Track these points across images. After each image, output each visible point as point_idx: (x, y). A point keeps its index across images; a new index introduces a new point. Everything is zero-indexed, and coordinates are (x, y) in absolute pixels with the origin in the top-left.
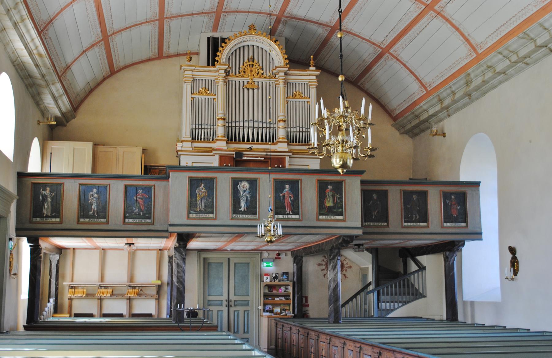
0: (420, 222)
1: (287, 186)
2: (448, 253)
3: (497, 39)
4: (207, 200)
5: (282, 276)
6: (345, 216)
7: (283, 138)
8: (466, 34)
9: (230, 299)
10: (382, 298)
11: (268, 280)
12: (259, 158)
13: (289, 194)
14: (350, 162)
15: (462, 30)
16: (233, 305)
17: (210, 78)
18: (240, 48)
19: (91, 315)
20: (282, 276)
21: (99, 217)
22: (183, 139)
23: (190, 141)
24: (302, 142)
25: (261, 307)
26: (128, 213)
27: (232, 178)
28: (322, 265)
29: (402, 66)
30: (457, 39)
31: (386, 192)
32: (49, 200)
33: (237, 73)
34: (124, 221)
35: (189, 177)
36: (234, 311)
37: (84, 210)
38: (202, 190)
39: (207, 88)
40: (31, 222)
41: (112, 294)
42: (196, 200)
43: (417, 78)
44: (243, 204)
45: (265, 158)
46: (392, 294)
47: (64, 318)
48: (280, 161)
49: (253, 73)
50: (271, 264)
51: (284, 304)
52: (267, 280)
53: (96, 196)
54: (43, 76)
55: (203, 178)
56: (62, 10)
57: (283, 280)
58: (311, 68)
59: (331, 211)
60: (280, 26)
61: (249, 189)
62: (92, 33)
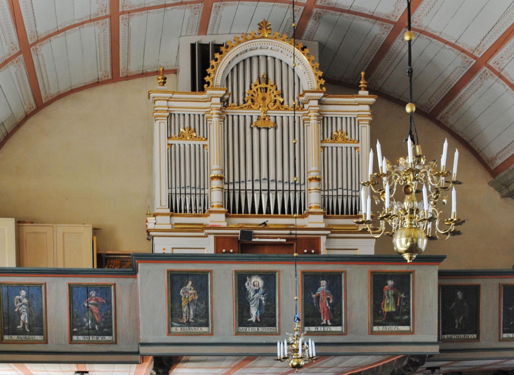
1: (323, 283)
4: (197, 305)
7: (316, 207)
12: (278, 240)
13: (327, 294)
14: (423, 242)
18: (244, 61)
21: (32, 333)
23: (167, 214)
31: (477, 288)
33: (241, 102)
34: (71, 339)
35: (169, 272)
38: (189, 291)
42: (181, 307)
44: (254, 311)
45: (288, 239)
48: (313, 243)
49: (267, 101)
53: (25, 301)
58: (361, 93)
59: (391, 319)
60: (311, 23)
61: (264, 288)
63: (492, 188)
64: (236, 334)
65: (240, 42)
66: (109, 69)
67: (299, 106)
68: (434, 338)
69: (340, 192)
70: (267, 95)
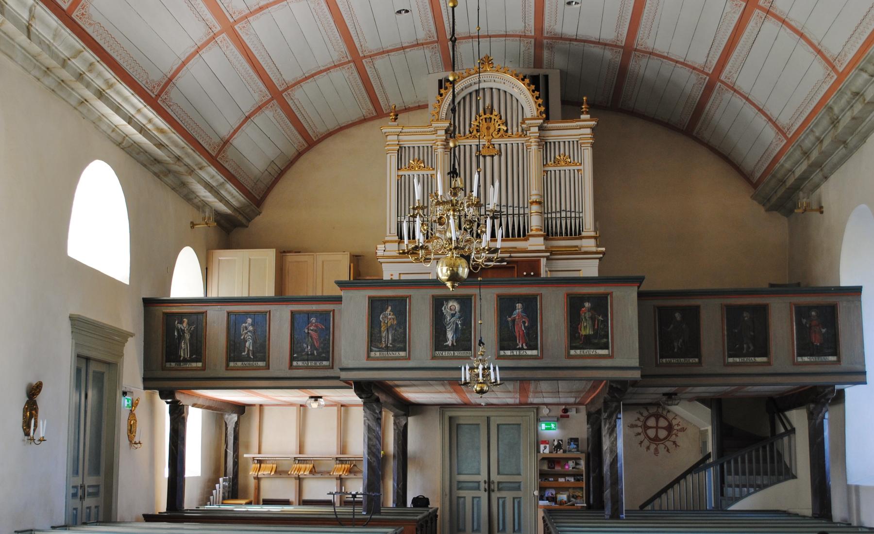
0: (755, 356)
2: (812, 406)
3: (858, 46)
4: (396, 330)
5: (569, 444)
6: (409, 352)
7: (537, 230)
8: (816, 43)
9: (492, 479)
10: (729, 479)
11: (547, 451)
14: (463, 271)
15: (808, 36)
16: (496, 489)
17: (425, 144)
18: (471, 94)
19: (286, 502)
20: (569, 444)
21: (256, 359)
22: (387, 239)
23: (395, 241)
24: (571, 234)
25: (536, 493)
26: (297, 353)
27: (433, 296)
28: (636, 426)
29: (744, 101)
30: (805, 53)
31: (696, 309)
32: (187, 336)
33: (467, 132)
34: (291, 365)
35: (369, 298)
36: (498, 498)
37: (234, 350)
38: (388, 316)
39: (421, 159)
40: (164, 369)
41: (313, 471)
42: (380, 332)
43: (770, 119)
44: (450, 335)
45: (508, 262)
46: (751, 473)
47: (239, 507)
48: (533, 265)
49: (491, 130)
50: (553, 426)
51: (574, 488)
52: (545, 450)
53: (251, 328)
54: (178, 159)
55: (390, 297)
56: (184, 64)
57: (570, 451)
58: (583, 117)
59: (588, 342)
60: (546, 54)
61: (460, 312)
62: (251, 90)
63: (755, 202)
64: (432, 359)
65: (464, 78)
66: (371, 107)
67: (524, 133)
68: (635, 363)
69: (563, 214)
70: (491, 125)
